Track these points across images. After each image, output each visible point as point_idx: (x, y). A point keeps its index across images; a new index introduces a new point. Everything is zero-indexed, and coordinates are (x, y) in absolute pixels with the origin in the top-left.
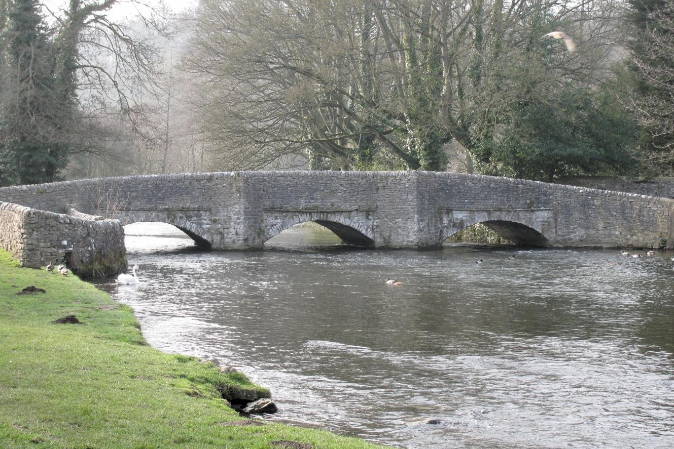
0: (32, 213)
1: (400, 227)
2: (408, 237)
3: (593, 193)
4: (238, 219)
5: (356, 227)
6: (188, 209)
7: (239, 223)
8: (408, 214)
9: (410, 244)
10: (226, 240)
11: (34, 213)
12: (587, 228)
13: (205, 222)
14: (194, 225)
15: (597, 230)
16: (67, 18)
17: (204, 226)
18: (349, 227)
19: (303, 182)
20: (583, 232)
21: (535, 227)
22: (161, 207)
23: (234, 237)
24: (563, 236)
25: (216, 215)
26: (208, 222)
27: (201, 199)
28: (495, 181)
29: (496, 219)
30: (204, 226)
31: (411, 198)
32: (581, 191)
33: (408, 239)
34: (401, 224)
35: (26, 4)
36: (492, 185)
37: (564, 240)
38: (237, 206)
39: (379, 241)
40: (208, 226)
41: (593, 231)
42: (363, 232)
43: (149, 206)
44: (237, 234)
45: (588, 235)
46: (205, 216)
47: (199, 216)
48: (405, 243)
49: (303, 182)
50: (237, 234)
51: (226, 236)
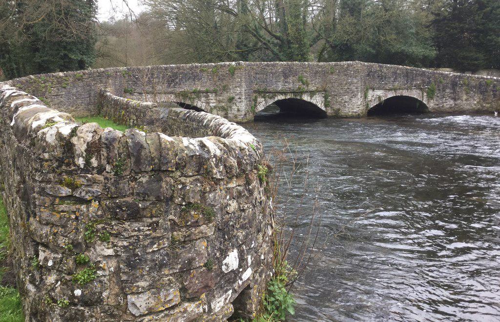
0: (80, 146)
1: (346, 102)
2: (353, 109)
3: (460, 76)
4: (240, 98)
6: (200, 92)
7: (240, 102)
8: (352, 92)
9: (354, 114)
10: (230, 115)
11: (93, 148)
12: (455, 99)
13: (212, 101)
14: (204, 104)
15: (462, 101)
16: (35, 125)
17: (211, 105)
18: (310, 103)
19: (280, 70)
20: (452, 102)
22: (178, 90)
23: (236, 113)
24: (438, 105)
25: (220, 96)
26: (214, 101)
27: (208, 84)
28: (400, 69)
29: (399, 95)
30: (211, 105)
32: (451, 75)
33: (352, 111)
35: (28, 283)
36: (398, 72)
37: (439, 107)
38: (239, 89)
39: (329, 111)
40: (214, 104)
41: (459, 102)
42: (319, 106)
43: (170, 90)
44: (238, 110)
45: (455, 105)
46: (212, 96)
47: (207, 97)
48: (350, 113)
49: (280, 70)
50: (238, 110)
51: (229, 112)
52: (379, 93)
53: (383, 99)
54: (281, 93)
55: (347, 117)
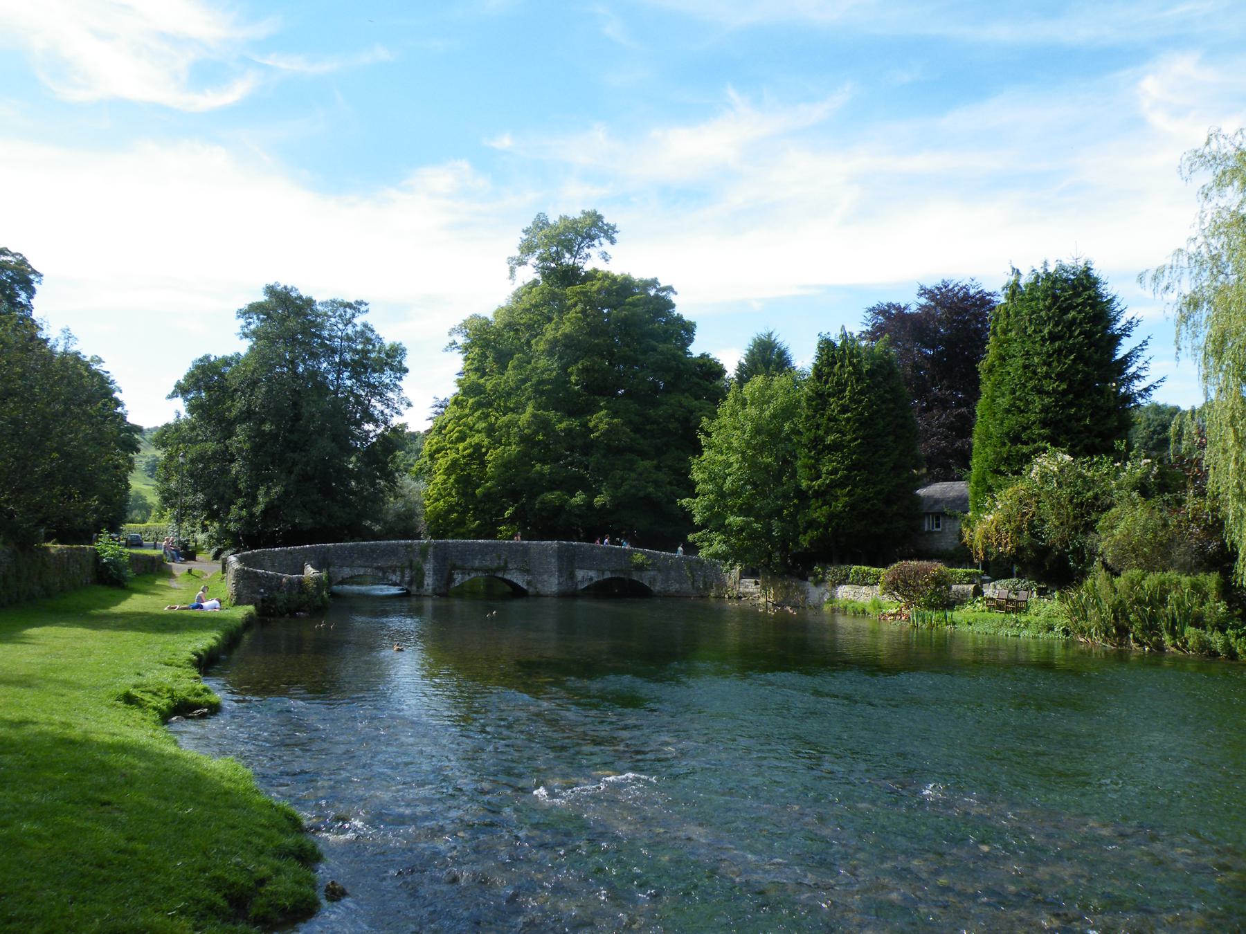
5: (515, 581)
21: (644, 582)
22: (375, 565)
31: (553, 560)
34: (546, 579)
39: (531, 590)
43: (367, 564)
52: (592, 574)
53: (595, 580)
54: (476, 570)
55: (547, 596)
